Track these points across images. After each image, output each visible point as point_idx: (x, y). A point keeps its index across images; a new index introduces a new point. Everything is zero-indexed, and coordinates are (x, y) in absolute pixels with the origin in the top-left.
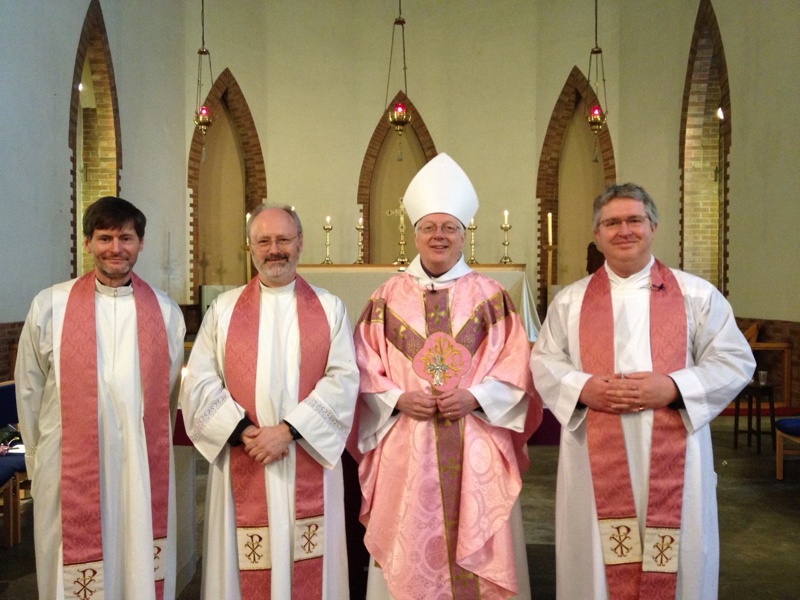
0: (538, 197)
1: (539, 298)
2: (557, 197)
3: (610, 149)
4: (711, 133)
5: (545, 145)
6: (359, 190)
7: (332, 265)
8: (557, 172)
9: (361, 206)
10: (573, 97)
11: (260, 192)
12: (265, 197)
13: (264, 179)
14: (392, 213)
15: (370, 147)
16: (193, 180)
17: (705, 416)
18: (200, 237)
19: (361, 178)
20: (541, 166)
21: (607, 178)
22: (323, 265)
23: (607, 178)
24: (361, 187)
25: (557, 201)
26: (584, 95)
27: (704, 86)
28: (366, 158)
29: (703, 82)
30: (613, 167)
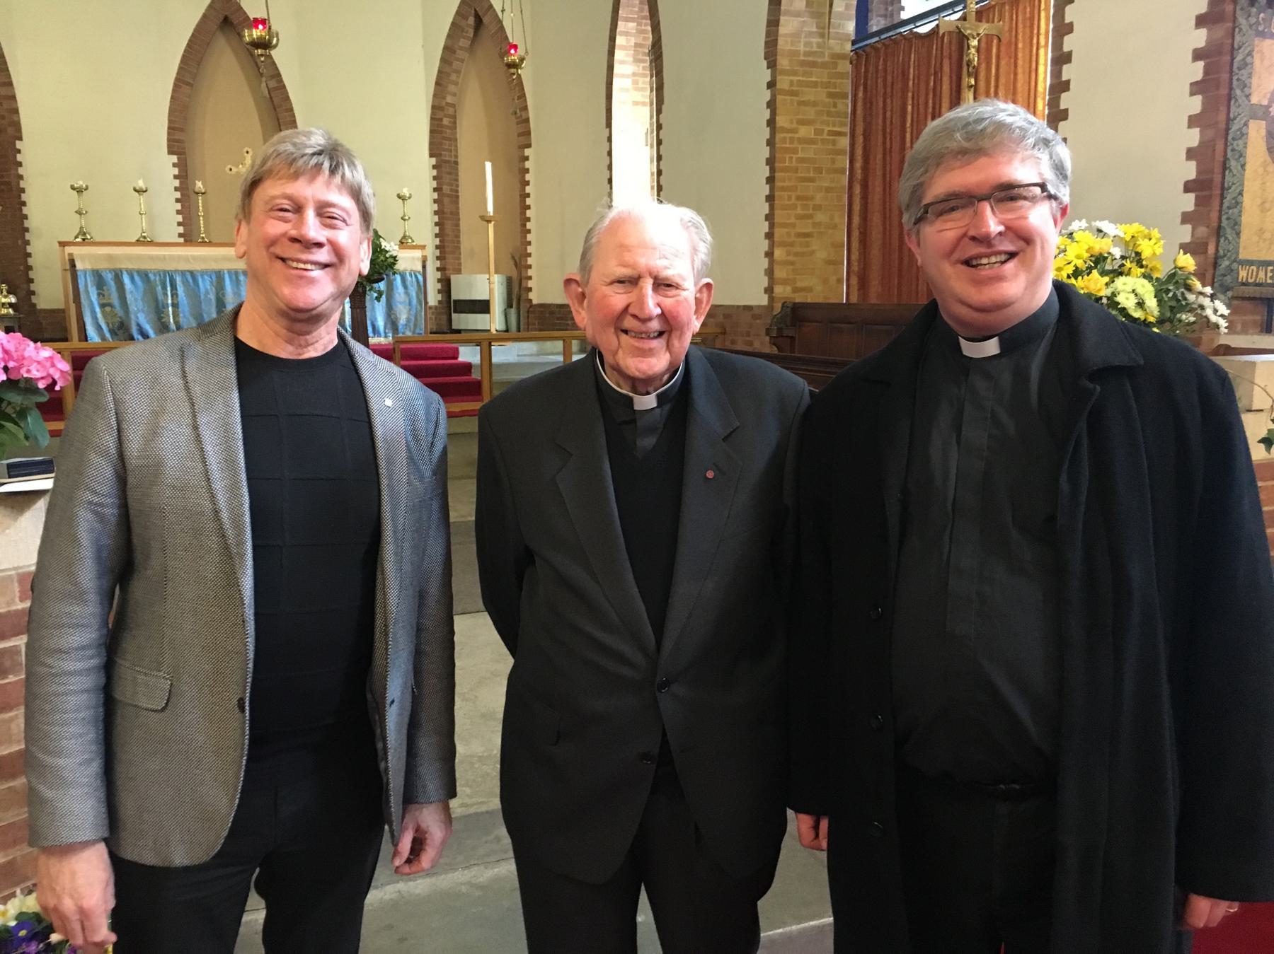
0: (431, 155)
1: (439, 292)
2: (456, 156)
3: (522, 96)
4: (640, 85)
5: (437, 84)
6: (169, 134)
7: (152, 243)
8: (455, 123)
9: (174, 159)
10: (471, 20)
11: (10, 130)
12: (21, 139)
13: (16, 111)
14: (234, 170)
15: (180, 68)
16: (177, 144)
17: (88, 762)
18: (519, 229)
19: (170, 115)
20: (433, 114)
21: (519, 135)
22: (139, 242)
23: (519, 135)
24: (171, 129)
25: (456, 163)
26: (485, 20)
27: (632, 25)
28: (175, 85)
29: (632, 20)
30: (527, 120)
